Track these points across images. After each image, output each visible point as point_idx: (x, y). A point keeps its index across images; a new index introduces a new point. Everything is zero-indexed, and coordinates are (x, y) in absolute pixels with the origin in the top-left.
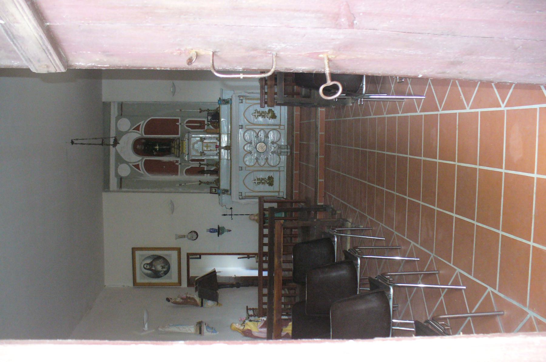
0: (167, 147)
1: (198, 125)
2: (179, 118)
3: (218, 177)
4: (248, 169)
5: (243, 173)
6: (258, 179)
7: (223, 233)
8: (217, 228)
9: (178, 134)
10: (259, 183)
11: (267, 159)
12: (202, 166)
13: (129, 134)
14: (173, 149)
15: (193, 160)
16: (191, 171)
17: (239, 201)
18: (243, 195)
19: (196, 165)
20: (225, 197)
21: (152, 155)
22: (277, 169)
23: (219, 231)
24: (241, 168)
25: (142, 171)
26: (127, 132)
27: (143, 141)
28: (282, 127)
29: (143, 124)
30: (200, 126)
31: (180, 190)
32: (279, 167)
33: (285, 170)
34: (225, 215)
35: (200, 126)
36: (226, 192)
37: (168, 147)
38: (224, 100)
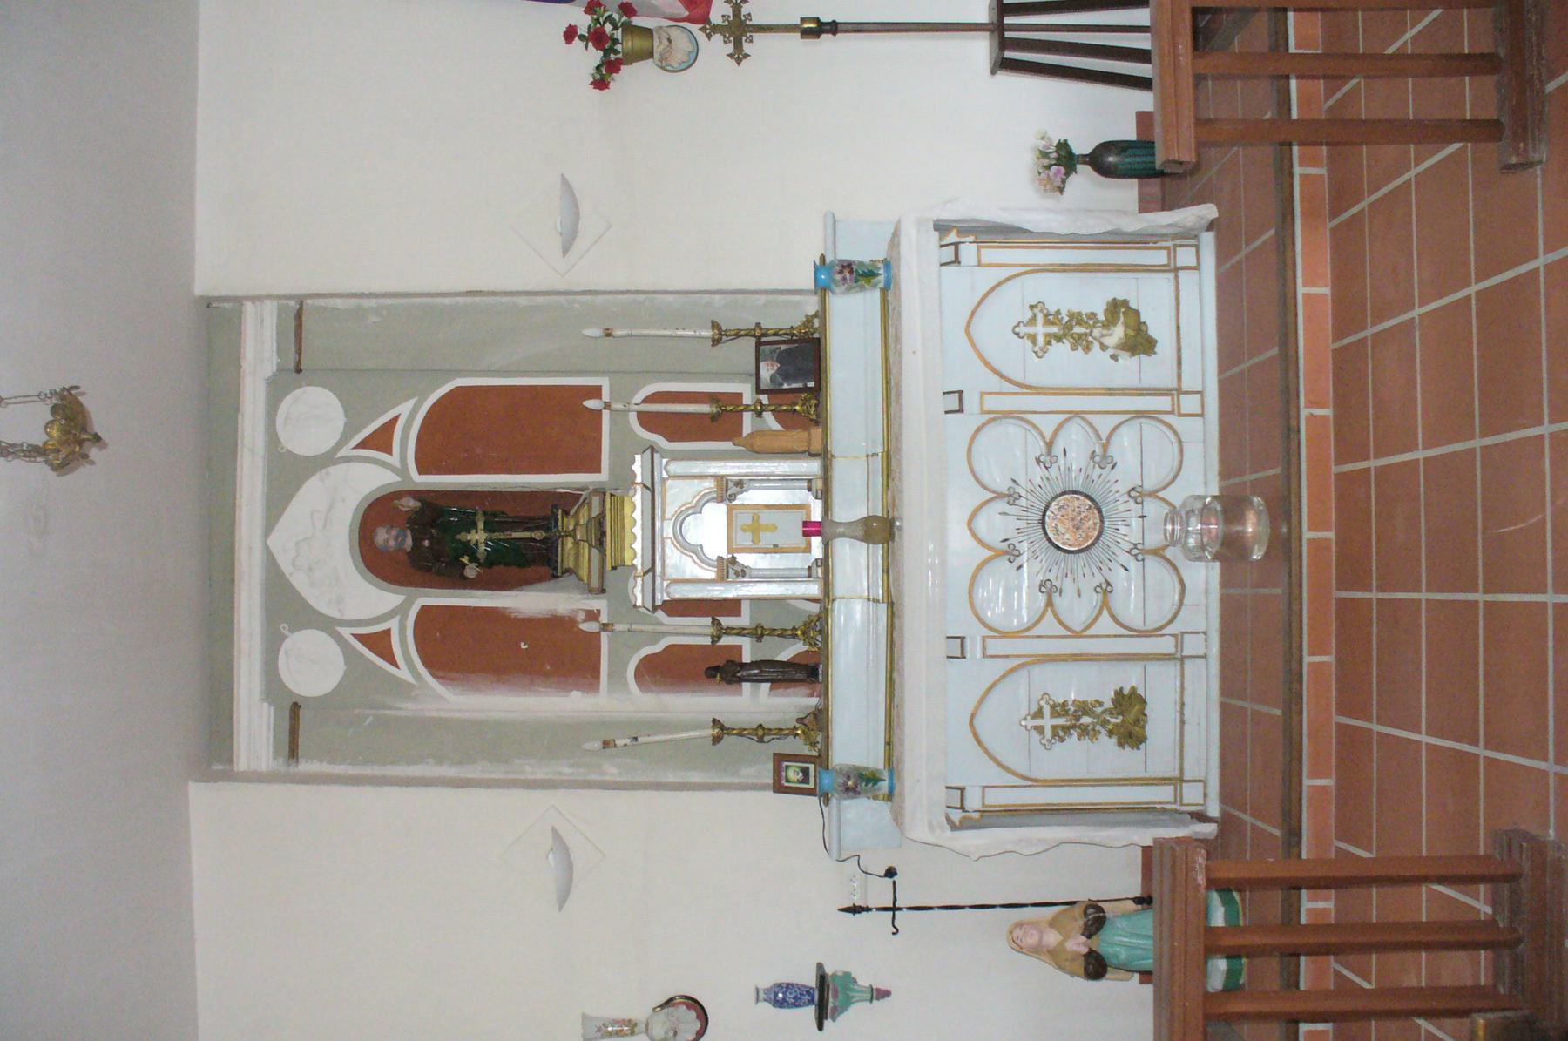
0: (530, 542)
1: (705, 408)
2: (604, 382)
3: (814, 701)
4: (996, 646)
5: (977, 672)
6: (1059, 709)
7: (844, 1008)
8: (811, 981)
9: (598, 470)
10: (1060, 733)
11: (1106, 589)
12: (726, 641)
13: (335, 471)
14: (569, 543)
15: (678, 607)
16: (667, 670)
17: (947, 837)
18: (973, 802)
19: (695, 632)
20: (860, 813)
21: (455, 578)
22: (1165, 645)
23: (824, 996)
24: (959, 648)
25: (408, 665)
26: (327, 460)
27: (410, 504)
28: (1190, 404)
29: (410, 414)
30: (713, 418)
31: (612, 772)
32: (1179, 638)
33: (1215, 650)
34: (855, 910)
35: (715, 422)
36: (861, 782)
37: (539, 535)
38: (847, 266)
